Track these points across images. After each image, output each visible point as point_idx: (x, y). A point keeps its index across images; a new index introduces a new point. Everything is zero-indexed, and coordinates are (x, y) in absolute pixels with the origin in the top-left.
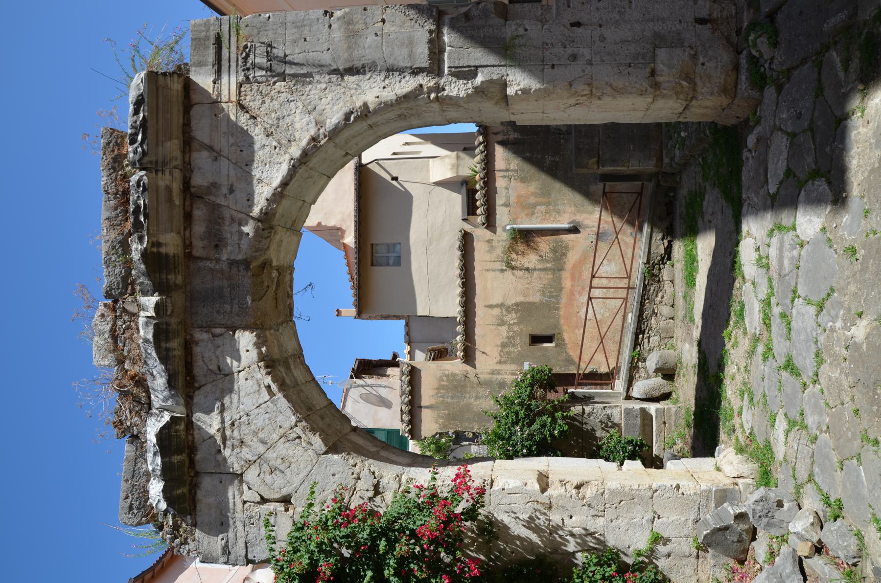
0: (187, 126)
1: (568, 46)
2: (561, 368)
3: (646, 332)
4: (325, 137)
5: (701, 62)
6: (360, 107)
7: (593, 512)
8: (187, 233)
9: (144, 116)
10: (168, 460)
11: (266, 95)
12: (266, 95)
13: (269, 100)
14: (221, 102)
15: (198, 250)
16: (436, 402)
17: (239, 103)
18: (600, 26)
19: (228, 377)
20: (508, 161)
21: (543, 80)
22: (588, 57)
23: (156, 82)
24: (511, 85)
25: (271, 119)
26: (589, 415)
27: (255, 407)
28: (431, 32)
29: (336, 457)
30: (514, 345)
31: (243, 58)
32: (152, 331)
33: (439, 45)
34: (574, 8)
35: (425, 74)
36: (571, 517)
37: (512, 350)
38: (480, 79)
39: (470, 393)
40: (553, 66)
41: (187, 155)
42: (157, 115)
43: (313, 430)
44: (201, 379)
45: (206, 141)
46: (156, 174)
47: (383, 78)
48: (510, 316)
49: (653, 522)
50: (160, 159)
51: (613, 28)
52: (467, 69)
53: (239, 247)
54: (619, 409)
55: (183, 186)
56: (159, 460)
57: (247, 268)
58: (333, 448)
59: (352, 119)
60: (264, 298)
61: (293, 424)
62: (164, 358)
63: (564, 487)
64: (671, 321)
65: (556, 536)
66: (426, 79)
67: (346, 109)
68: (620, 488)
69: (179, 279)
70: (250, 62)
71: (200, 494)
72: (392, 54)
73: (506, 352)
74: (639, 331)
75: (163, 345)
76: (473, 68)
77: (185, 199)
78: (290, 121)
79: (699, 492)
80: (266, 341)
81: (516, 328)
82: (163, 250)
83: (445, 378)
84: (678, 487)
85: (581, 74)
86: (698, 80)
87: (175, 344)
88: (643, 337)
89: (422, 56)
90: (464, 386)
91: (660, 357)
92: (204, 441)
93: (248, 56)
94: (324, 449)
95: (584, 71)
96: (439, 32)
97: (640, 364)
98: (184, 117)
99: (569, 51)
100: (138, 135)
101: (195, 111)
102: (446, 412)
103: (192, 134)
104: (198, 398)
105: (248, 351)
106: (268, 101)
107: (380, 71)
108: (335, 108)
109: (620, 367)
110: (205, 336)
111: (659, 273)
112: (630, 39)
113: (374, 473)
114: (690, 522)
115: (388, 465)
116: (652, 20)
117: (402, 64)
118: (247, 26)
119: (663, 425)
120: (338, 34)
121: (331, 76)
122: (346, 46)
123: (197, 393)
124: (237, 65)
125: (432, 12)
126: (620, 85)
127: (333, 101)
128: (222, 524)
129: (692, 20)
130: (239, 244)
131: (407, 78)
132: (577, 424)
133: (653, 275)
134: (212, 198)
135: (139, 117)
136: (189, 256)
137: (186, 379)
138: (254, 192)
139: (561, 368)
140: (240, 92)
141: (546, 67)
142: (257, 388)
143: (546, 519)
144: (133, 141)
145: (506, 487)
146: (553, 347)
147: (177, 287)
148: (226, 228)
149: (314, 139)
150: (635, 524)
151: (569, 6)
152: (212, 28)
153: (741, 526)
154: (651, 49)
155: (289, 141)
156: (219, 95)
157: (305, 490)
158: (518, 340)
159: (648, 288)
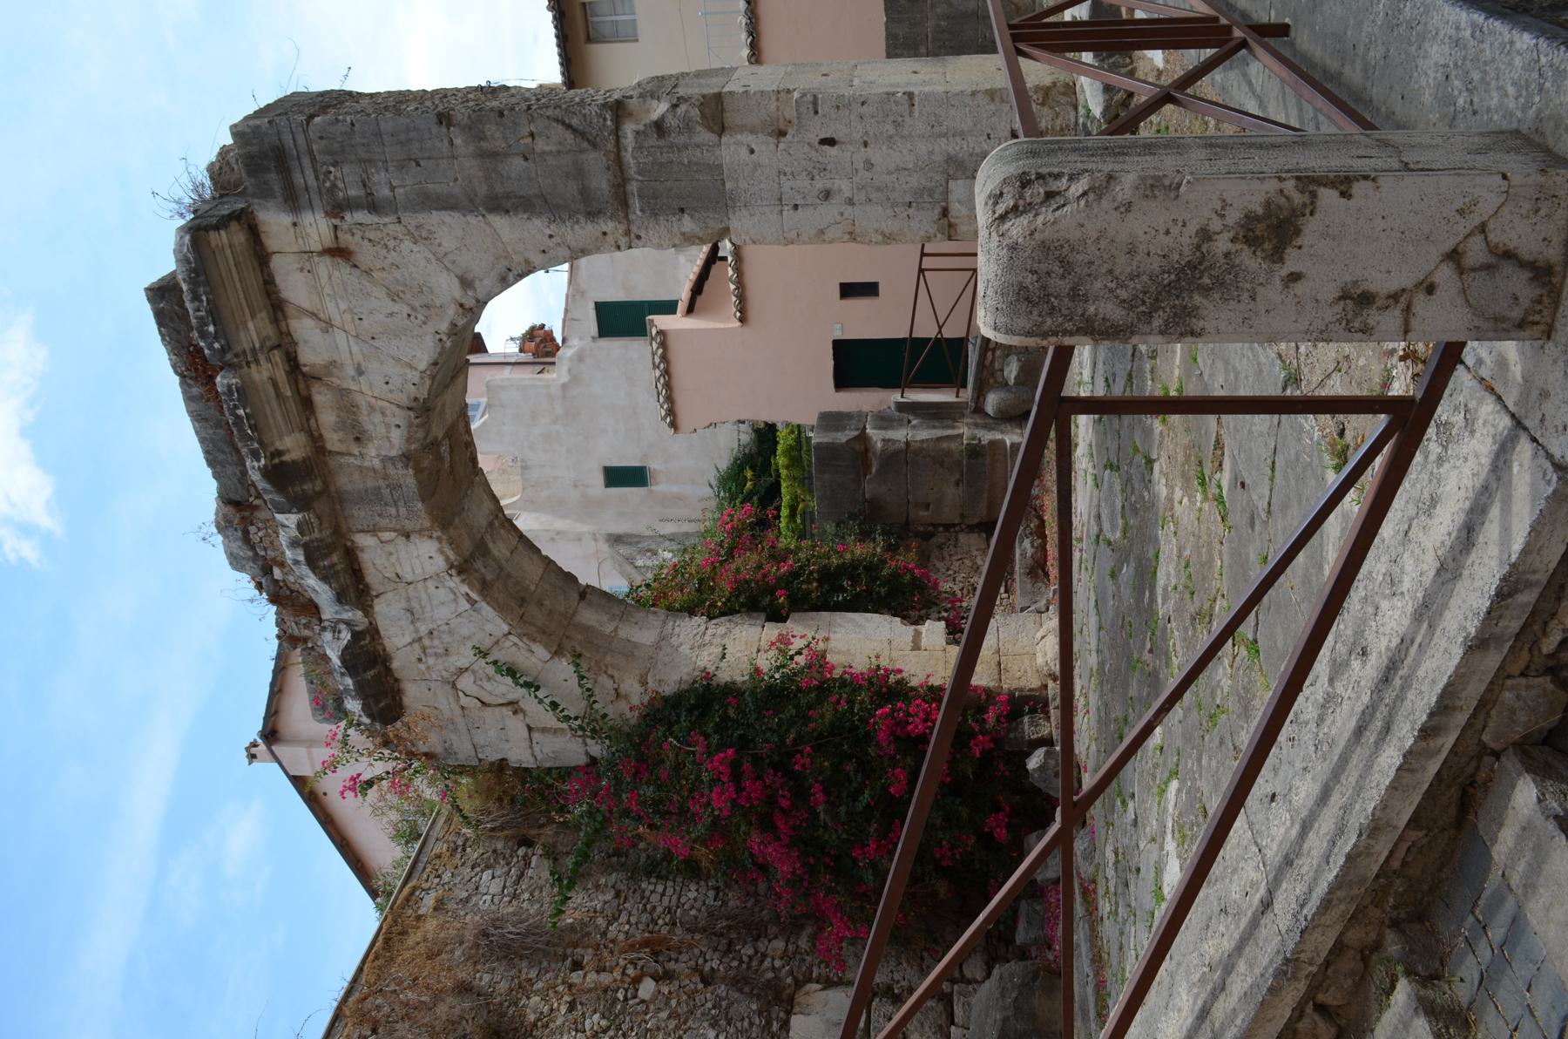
18: (866, 144)
22: (848, 194)
40: (796, 207)
41: (283, 324)
51: (884, 148)
82: (287, 458)
95: (842, 214)
99: (820, 184)
116: (945, 135)
151: (816, 113)
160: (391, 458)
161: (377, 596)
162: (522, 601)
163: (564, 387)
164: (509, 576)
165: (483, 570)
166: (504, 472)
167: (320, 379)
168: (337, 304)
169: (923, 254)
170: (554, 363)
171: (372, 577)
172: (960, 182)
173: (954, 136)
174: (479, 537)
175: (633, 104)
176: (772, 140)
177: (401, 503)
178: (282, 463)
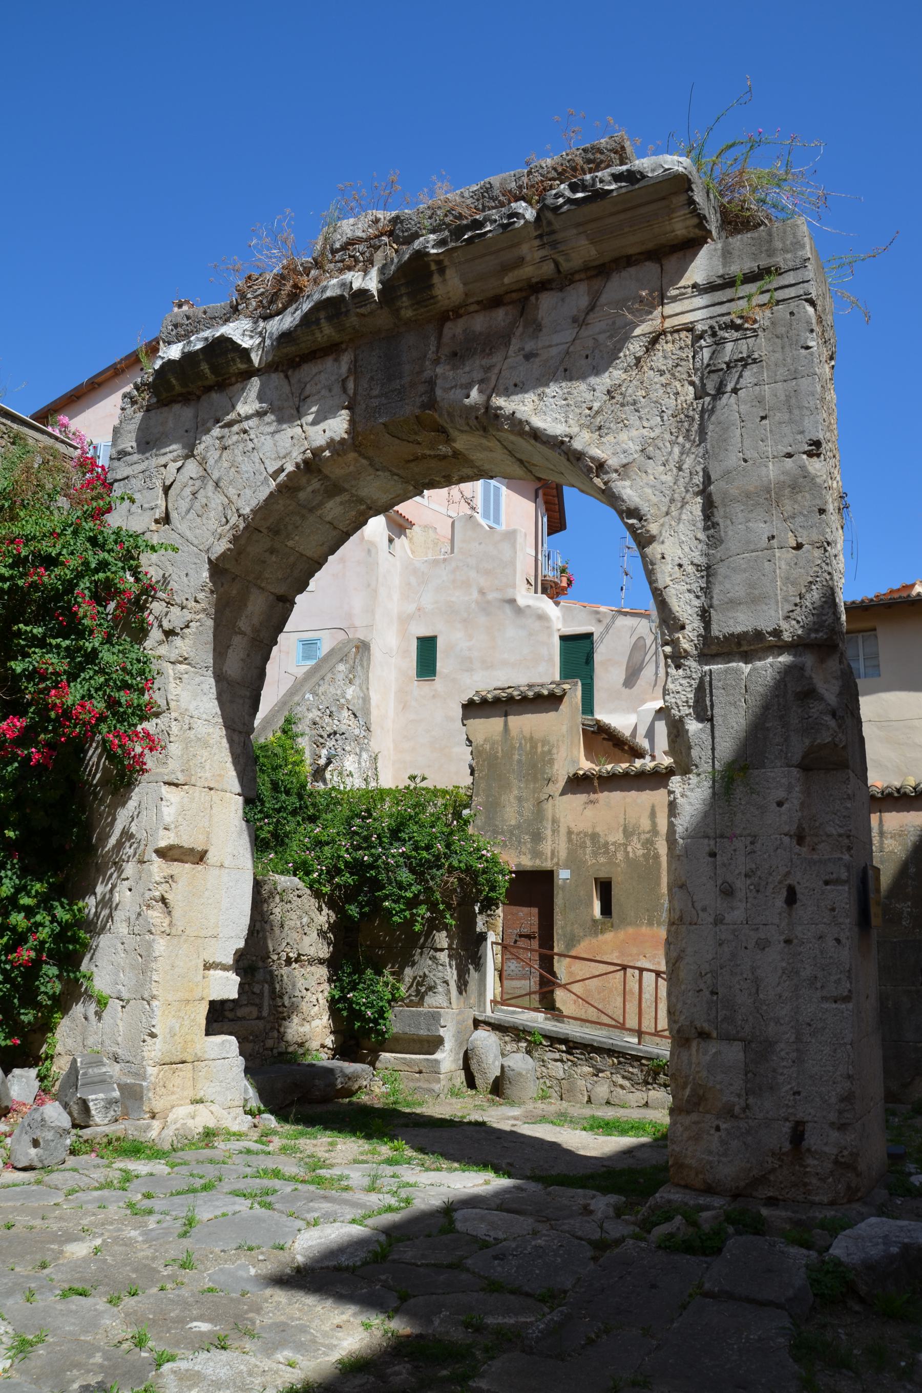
0: (627, 261)
1: (748, 882)
2: (562, 928)
3: (571, 1057)
4: (606, 483)
5: (721, 1124)
6: (648, 531)
7: (133, 917)
9: (612, 190)
10: (201, 357)
11: (673, 375)
12: (673, 375)
13: (664, 381)
14: (663, 304)
15: (454, 330)
16: (513, 738)
17: (660, 334)
18: (788, 942)
19: (294, 412)
20: (899, 834)
21: (689, 837)
22: (728, 918)
23: (675, 193)
24: (684, 783)
25: (634, 392)
26: (433, 958)
27: (261, 456)
28: (777, 633)
29: (206, 574)
30: (595, 854)
31: (732, 321)
32: (334, 295)
33: (756, 651)
34: (823, 893)
35: (702, 631)
36: (130, 890)
37: (588, 850)
38: (693, 726)
39: (526, 788)
40: (713, 855)
41: (583, 276)
42: (619, 212)
43: (235, 539)
44: (296, 376)
45: (603, 299)
46: (536, 237)
47: (696, 561)
48: (639, 846)
49: (118, 998)
50: (559, 236)
51: (784, 964)
52: (708, 703)
53: (452, 388)
54: (445, 1004)
55: (537, 283)
56: (199, 346)
57: (424, 406)
58: (217, 569)
59: (631, 521)
60: (397, 441)
61: (242, 512)
62: (307, 320)
63: (163, 880)
64: (586, 1099)
65: (112, 870)
66: (693, 635)
67: (645, 508)
68: (154, 955)
69: (408, 313)
70: (727, 335)
71: (176, 407)
72: (734, 570)
73: (584, 842)
74: (571, 1044)
75: (322, 315)
76: (709, 713)
77: (520, 290)
78: (631, 422)
79: (144, 1063)
80: (339, 455)
81: (620, 856)
82: (436, 279)
83: (546, 748)
84: (153, 1035)
86: (694, 1117)
87: (326, 332)
88: (563, 1052)
89: (731, 622)
90: (535, 779)
91: (520, 1074)
92: (230, 398)
93: (738, 328)
94: (213, 558)
95: (704, 909)
96: (781, 648)
97: (525, 1045)
98: (640, 254)
99: (740, 884)
100: (583, 191)
101: (651, 268)
102: (500, 754)
103: (614, 274)
104: (276, 378)
105: (324, 431)
106: (663, 380)
107: (707, 555)
108: (649, 491)
109: (563, 1022)
110: (344, 368)
111: (660, 1085)
112: (761, 996)
113: (187, 626)
114: (115, 1049)
115: (210, 647)
116: (798, 1039)
117: (716, 591)
118: (792, 314)
119: (417, 1070)
120: (772, 471)
121: (701, 474)
122: (751, 488)
123: (282, 375)
124: (723, 315)
125: (817, 631)
126: (682, 975)
127: (659, 486)
128: (148, 443)
129: (800, 1116)
130: (456, 386)
131: (697, 603)
132: (422, 941)
133: (657, 1074)
135: (610, 183)
136: (444, 318)
137: (296, 356)
138: (526, 392)
139: (562, 928)
140: (678, 331)
141: (712, 842)
142: (281, 455)
143: (129, 857)
144: (574, 188)
145: (164, 803)
146: (592, 915)
147: (396, 312)
148: (477, 362)
149: (601, 466)
150: (117, 975)
151: (827, 883)
152: (789, 256)
153: (76, 1107)
155: (600, 428)
156: (674, 299)
157: (175, 539)
158: (602, 860)
159: (636, 1064)
160: (433, 390)
161: (287, 377)
162: (275, 531)
163: (512, 601)
164: (303, 517)
165: (309, 489)
166: (436, 544)
167: (522, 314)
168: (604, 332)
169: (641, 970)
170: (536, 592)
171: (309, 370)
172: (741, 1055)
173: (798, 1050)
174: (347, 486)
175: (833, 664)
176: (793, 829)
177: (384, 400)
178: (430, 274)
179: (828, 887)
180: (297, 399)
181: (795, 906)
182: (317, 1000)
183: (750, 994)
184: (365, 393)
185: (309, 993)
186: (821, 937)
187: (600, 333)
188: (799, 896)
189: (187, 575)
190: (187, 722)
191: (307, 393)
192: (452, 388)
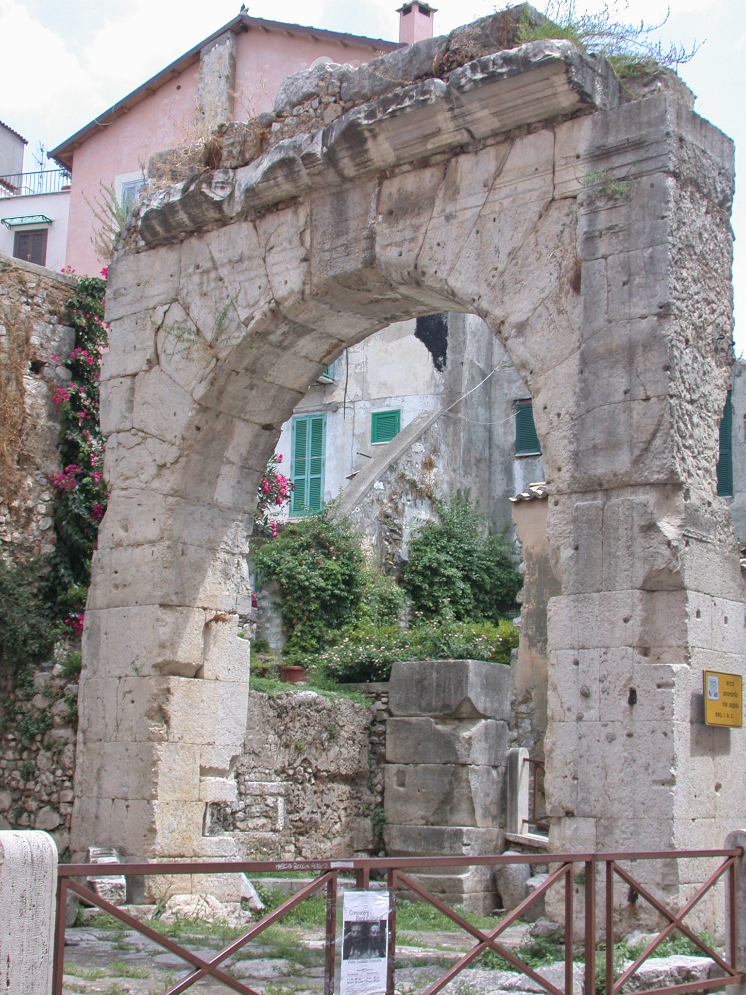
8: (406, 167)
15: (392, 187)
18: (630, 735)
22: (587, 715)
36: (133, 702)
40: (577, 663)
45: (508, 166)
51: (626, 754)
77: (443, 152)
82: (370, 144)
85: (566, 706)
95: (569, 709)
99: (595, 688)
103: (518, 140)
110: (302, 220)
112: (609, 780)
123: (251, 224)
134: (441, 194)
135: (502, 67)
142: (251, 303)
148: (408, 222)
151: (659, 686)
152: (652, 130)
154: (594, 813)
161: (255, 227)
165: (279, 332)
167: (444, 178)
171: (271, 222)
173: (635, 825)
179: (659, 690)
180: (263, 250)
181: (635, 706)
182: (339, 818)
183: (600, 779)
184: (319, 247)
185: (329, 811)
186: (653, 732)
187: (505, 198)
188: (639, 697)
189: (175, 414)
190: (180, 549)
191: (270, 245)
192: (388, 245)
